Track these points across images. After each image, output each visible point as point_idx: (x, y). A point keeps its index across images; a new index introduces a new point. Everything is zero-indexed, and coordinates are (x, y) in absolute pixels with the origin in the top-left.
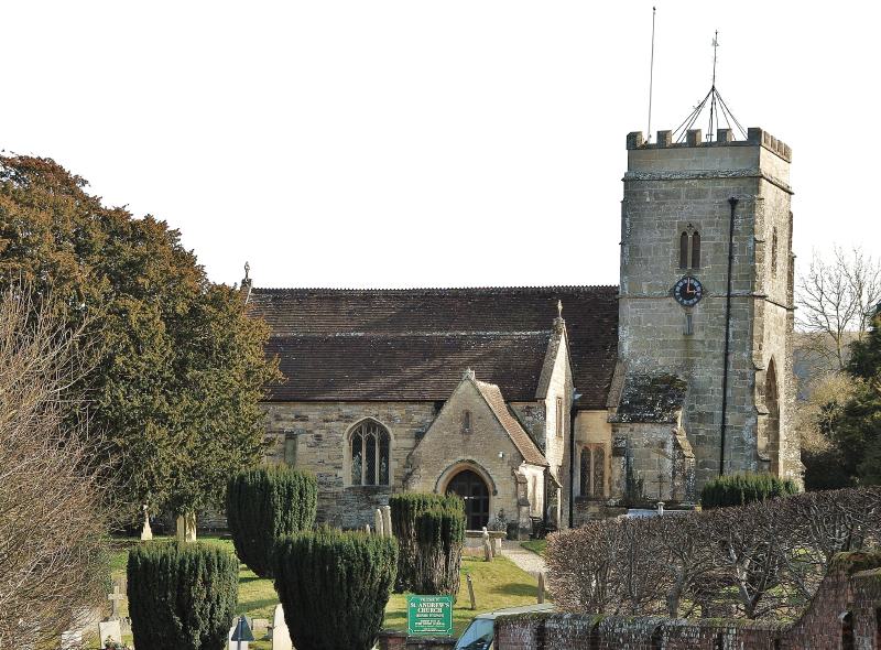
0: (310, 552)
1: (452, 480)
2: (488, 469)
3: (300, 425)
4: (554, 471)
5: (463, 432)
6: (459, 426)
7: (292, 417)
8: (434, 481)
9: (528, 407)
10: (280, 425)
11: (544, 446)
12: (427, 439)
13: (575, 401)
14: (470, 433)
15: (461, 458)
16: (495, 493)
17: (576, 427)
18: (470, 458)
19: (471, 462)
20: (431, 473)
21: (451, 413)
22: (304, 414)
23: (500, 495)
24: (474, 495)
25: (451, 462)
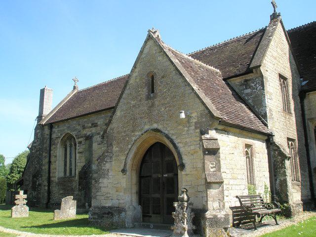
0: (238, 222)
1: (144, 161)
2: (174, 137)
3: (94, 130)
4: (280, 139)
5: (148, 98)
6: (145, 91)
7: (90, 125)
8: (123, 158)
9: (246, 81)
10: (85, 132)
11: (265, 116)
12: (118, 113)
13: (302, 86)
14: (155, 97)
15: (147, 127)
16: (183, 166)
17: (306, 108)
18: (155, 126)
19: (157, 130)
20: (121, 150)
21: (138, 80)
22: (96, 122)
23: (188, 167)
24: (168, 172)
25: (138, 133)
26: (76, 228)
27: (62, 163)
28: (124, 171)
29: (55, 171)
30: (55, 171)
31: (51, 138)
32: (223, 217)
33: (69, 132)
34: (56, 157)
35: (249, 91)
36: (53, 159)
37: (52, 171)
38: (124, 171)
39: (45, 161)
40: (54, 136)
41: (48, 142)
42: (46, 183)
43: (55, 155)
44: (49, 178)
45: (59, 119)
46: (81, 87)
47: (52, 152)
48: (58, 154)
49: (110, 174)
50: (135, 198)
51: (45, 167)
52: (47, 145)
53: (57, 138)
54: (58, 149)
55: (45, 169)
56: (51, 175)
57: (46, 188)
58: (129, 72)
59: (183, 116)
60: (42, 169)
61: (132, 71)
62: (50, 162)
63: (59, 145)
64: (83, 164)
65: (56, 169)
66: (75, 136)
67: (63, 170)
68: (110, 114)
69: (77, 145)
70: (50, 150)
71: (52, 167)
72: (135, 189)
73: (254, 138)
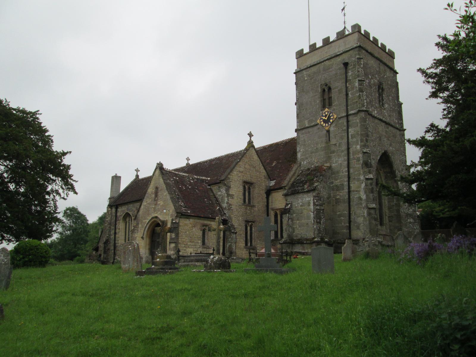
26: (151, 276)
27: (124, 234)
28: (142, 238)
29: (118, 239)
30: (118, 239)
31: (116, 216)
32: (174, 257)
33: (128, 212)
34: (119, 229)
35: (219, 193)
36: (117, 231)
37: (117, 239)
38: (142, 238)
39: (113, 232)
40: (118, 214)
41: (114, 219)
42: (112, 248)
43: (119, 228)
44: (115, 243)
45: (121, 202)
46: (191, 162)
47: (117, 226)
48: (121, 227)
49: (137, 239)
50: (147, 251)
51: (113, 237)
52: (113, 220)
53: (120, 216)
54: (121, 224)
55: (112, 238)
56: (116, 242)
57: (113, 251)
58: (151, 174)
59: (46, 217)
60: (110, 238)
61: (153, 174)
62: (115, 233)
63: (121, 221)
64: (324, 245)
65: (119, 237)
66: (131, 215)
67: (124, 239)
68: (138, 204)
69: (133, 221)
70: (116, 224)
71: (117, 236)
72: (148, 247)
73: (211, 221)
